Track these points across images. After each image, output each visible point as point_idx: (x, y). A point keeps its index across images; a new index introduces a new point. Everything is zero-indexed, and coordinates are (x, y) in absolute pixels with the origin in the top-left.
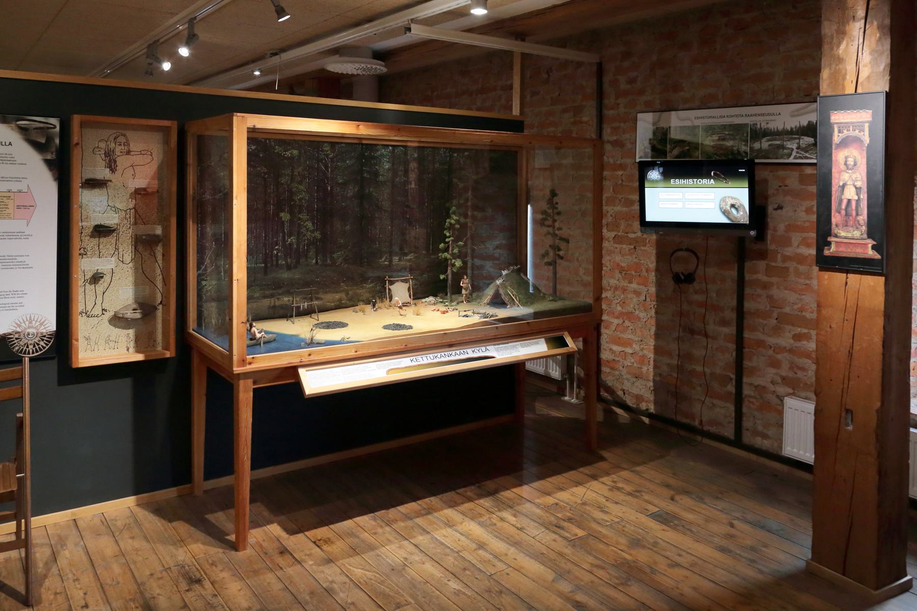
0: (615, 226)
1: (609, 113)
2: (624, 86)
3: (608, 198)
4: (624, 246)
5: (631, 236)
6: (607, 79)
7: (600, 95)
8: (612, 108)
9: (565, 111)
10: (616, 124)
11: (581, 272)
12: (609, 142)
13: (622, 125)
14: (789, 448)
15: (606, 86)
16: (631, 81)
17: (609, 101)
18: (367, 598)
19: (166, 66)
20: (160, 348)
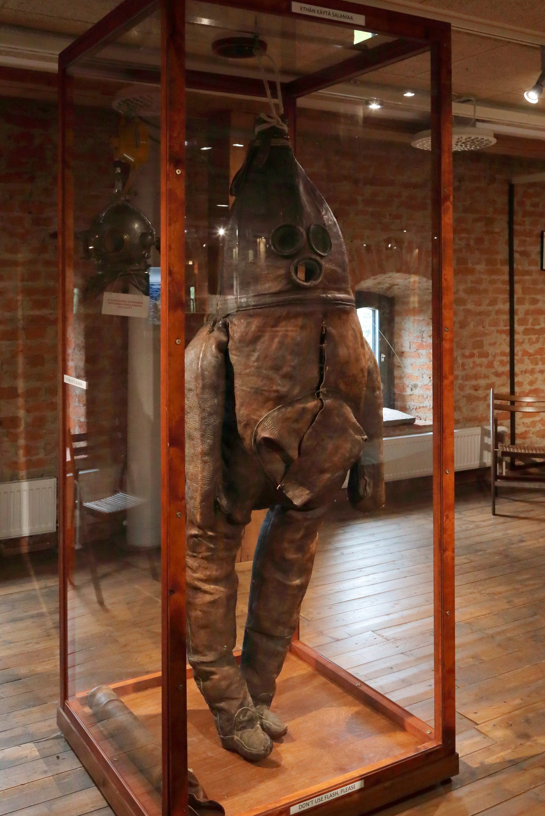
0: (523, 322)
1: (516, 227)
2: (529, 208)
3: (518, 298)
4: (532, 336)
5: (537, 327)
6: (516, 200)
7: (511, 213)
8: (520, 224)
9: (476, 220)
10: (523, 238)
11: (496, 364)
12: (517, 252)
13: (528, 239)
14: (476, 463)
15: (516, 207)
16: (535, 205)
17: (518, 218)
18: (470, 722)
19: (191, 263)
20: (195, 658)
